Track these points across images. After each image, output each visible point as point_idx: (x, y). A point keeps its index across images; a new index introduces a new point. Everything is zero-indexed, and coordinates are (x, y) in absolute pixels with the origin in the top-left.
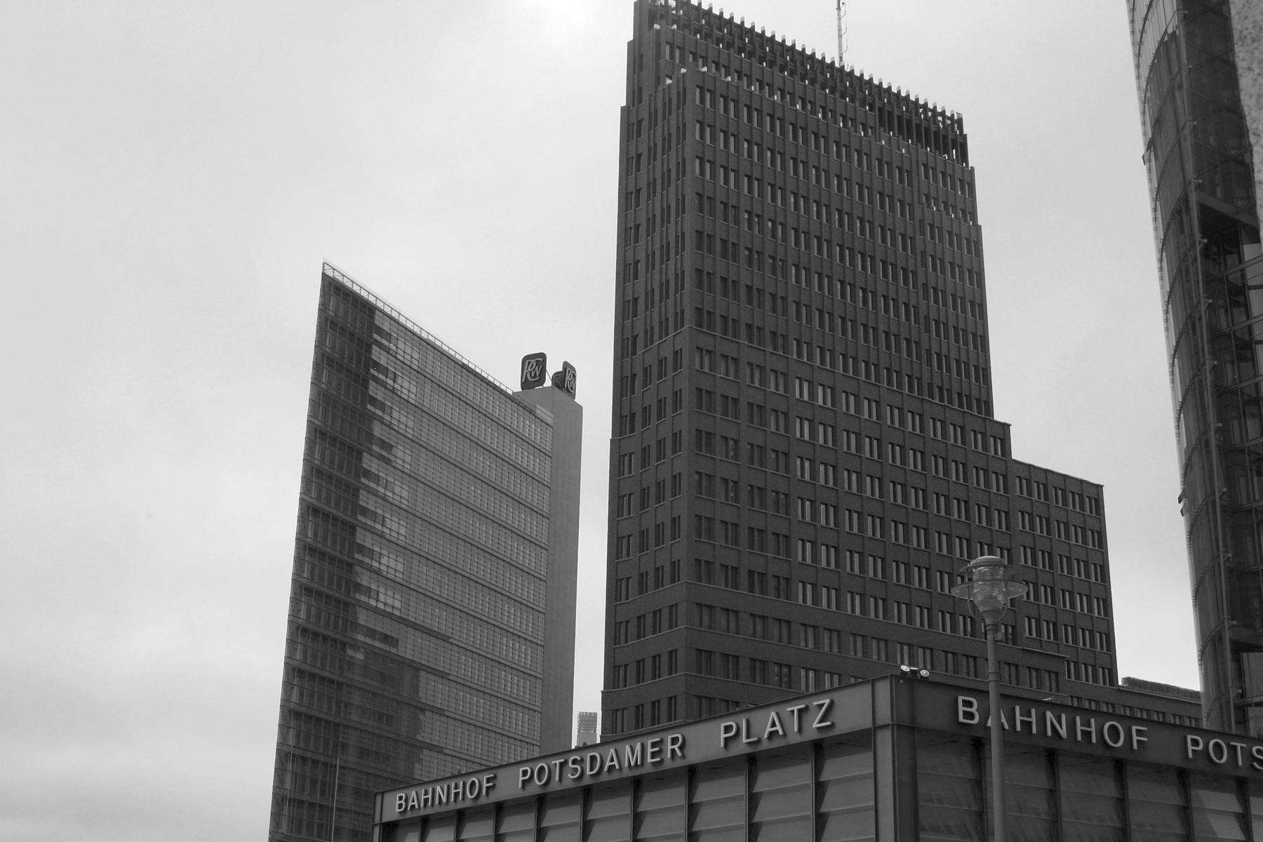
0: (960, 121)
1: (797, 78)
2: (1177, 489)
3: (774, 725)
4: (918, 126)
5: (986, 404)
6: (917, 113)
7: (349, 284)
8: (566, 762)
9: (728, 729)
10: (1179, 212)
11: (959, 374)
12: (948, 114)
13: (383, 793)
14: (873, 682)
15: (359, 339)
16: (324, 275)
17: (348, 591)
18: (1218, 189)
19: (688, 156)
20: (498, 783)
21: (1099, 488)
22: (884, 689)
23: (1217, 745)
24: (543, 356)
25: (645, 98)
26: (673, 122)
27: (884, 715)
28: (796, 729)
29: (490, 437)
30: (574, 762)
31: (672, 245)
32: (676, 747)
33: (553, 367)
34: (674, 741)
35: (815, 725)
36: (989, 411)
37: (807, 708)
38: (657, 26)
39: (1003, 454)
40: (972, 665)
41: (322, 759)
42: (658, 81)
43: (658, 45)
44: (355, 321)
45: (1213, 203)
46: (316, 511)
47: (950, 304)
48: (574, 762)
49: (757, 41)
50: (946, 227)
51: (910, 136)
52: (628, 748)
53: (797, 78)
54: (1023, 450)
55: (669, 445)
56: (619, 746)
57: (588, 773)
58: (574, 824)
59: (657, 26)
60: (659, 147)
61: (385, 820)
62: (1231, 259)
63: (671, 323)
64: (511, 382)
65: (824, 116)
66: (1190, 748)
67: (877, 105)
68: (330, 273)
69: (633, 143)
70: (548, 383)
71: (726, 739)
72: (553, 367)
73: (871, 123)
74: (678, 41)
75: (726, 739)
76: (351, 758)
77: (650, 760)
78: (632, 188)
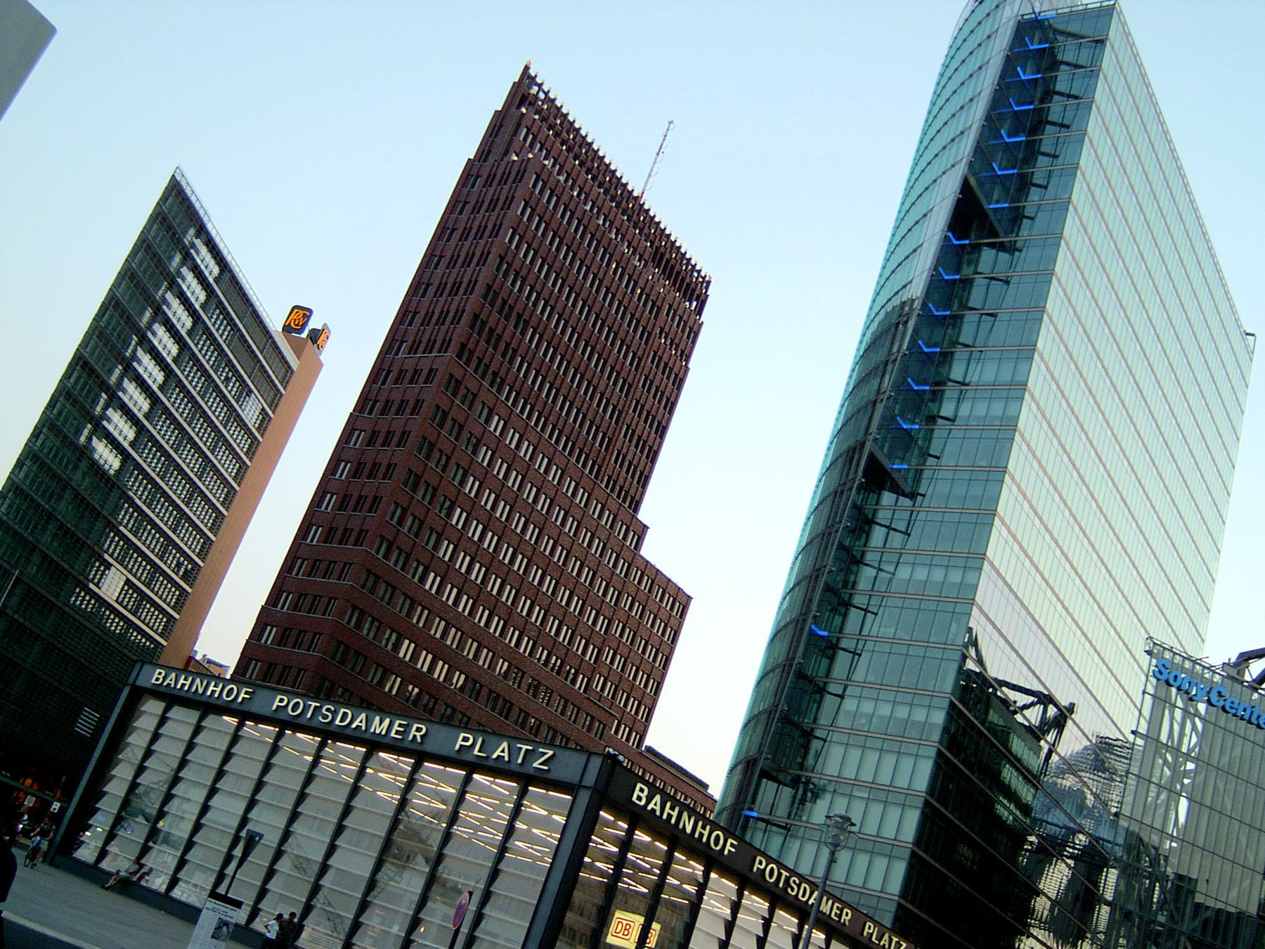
0: (709, 283)
1: (571, 155)
4: (678, 273)
5: (636, 505)
6: (691, 276)
7: (189, 192)
8: (321, 707)
10: (854, 450)
11: (627, 472)
12: (703, 274)
13: (144, 663)
14: (590, 754)
15: (174, 234)
18: (887, 445)
19: (506, 223)
21: (690, 598)
22: (596, 763)
23: (772, 869)
24: (310, 311)
25: (491, 160)
26: (505, 191)
27: (590, 779)
28: (520, 761)
30: (328, 710)
31: (464, 285)
32: (418, 735)
33: (314, 323)
34: (419, 730)
35: (535, 765)
36: (636, 510)
38: (524, 110)
39: (636, 548)
40: (407, 606)
42: (506, 153)
43: (519, 125)
44: (176, 216)
45: (880, 456)
46: (86, 364)
47: (643, 417)
48: (328, 710)
49: (553, 111)
50: (665, 358)
51: (679, 290)
52: (378, 718)
53: (571, 155)
54: (650, 551)
56: (371, 714)
57: (337, 722)
60: (486, 204)
61: (140, 683)
62: (873, 497)
63: (437, 346)
64: (275, 320)
65: (579, 195)
66: (757, 865)
67: (657, 243)
68: (178, 178)
69: (466, 190)
70: (304, 335)
72: (314, 323)
73: (646, 257)
77: (393, 734)
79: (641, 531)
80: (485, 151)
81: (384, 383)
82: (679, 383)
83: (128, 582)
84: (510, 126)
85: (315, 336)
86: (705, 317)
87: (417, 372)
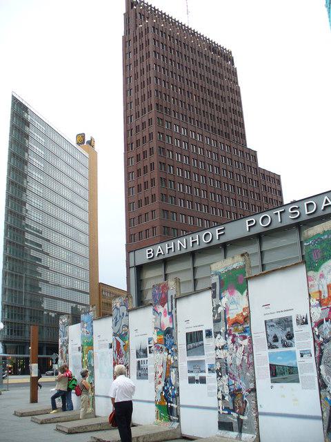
0: (231, 52)
2: (125, 243)
3: (160, 251)
9: (249, 222)
16: (13, 96)
17: (23, 241)
20: (226, 231)
26: (144, 40)
29: (69, 172)
33: (87, 139)
36: (246, 145)
37: (284, 211)
41: (19, 274)
42: (136, 26)
46: (10, 242)
55: (148, 153)
58: (258, 266)
59: (135, 7)
68: (14, 94)
71: (219, 235)
72: (87, 139)
74: (143, 13)
75: (249, 227)
76: (28, 273)
78: (128, 63)
79: (253, 155)
80: (127, 31)
81: (131, 135)
82: (238, 93)
83: (41, 233)
84: (132, 16)
85: (91, 143)
86: (236, 66)
87: (143, 124)
